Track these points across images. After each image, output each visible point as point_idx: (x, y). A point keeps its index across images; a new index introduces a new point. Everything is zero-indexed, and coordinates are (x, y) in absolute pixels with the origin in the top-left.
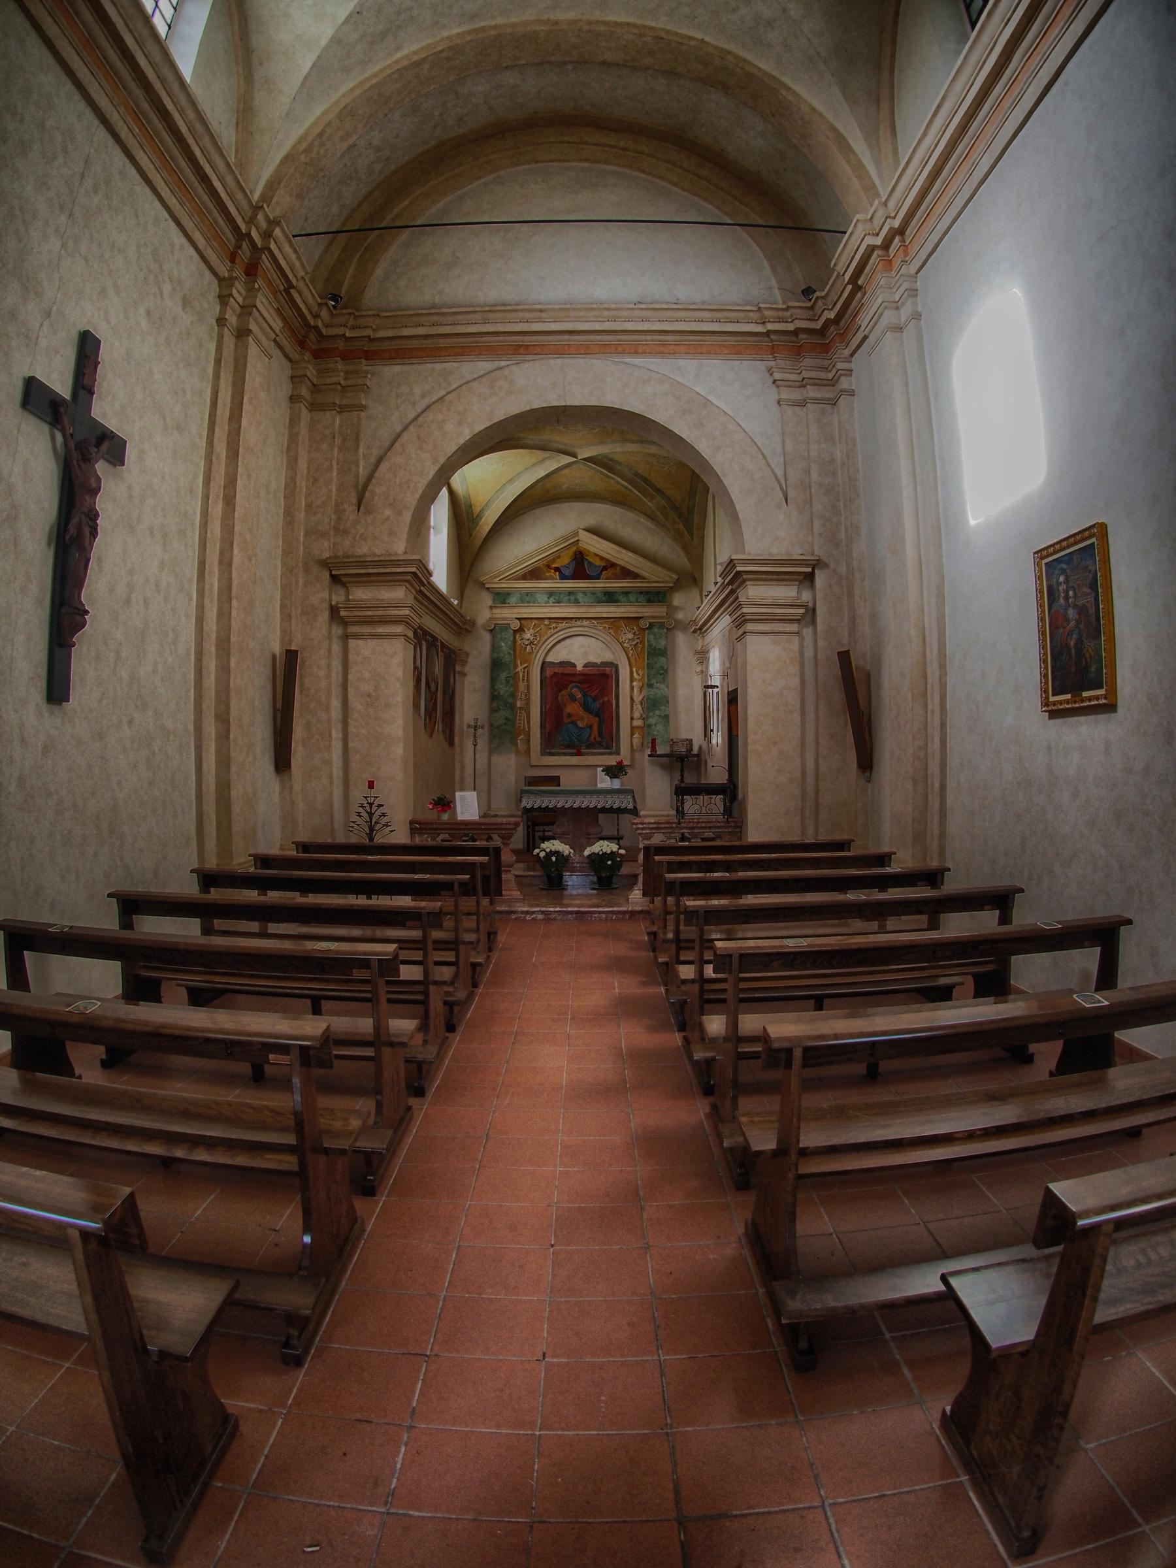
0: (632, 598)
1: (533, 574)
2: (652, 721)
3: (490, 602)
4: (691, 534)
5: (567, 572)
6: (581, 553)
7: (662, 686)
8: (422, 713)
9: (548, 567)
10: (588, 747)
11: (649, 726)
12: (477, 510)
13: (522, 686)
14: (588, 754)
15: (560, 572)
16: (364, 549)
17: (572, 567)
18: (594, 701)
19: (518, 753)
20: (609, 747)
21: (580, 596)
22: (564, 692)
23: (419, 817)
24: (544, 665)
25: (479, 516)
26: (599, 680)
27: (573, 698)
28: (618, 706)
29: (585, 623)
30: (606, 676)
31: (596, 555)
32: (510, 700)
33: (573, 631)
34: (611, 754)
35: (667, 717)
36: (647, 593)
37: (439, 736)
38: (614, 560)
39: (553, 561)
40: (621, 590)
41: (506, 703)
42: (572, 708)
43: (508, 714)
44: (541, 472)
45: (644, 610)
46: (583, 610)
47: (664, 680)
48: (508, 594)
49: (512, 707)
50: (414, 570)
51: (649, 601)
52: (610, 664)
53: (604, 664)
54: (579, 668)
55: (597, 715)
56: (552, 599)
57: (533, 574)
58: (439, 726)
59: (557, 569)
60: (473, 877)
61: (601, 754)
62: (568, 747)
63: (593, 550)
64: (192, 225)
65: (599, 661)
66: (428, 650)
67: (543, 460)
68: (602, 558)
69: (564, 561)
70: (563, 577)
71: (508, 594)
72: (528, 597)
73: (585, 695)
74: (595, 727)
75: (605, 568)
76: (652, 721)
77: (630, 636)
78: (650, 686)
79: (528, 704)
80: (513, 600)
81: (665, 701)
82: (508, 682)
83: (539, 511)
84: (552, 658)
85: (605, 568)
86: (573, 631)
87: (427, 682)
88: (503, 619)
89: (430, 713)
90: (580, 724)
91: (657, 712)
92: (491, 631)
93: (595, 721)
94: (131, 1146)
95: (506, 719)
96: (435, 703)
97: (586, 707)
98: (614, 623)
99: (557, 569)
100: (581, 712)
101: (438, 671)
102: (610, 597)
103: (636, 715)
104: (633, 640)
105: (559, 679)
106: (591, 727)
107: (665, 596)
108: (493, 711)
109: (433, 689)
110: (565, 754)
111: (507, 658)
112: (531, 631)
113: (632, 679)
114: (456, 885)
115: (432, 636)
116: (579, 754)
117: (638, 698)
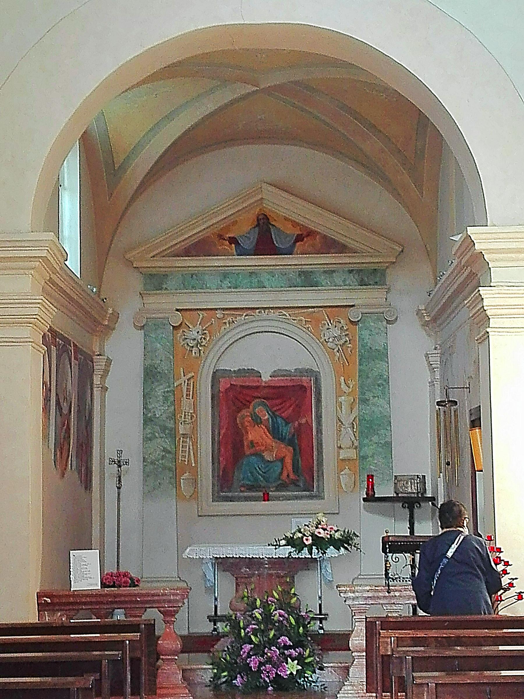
0: (338, 279)
1: (200, 248)
2: (368, 451)
3: (140, 287)
4: (419, 185)
5: (248, 244)
6: (266, 218)
7: (381, 402)
8: (52, 446)
9: (221, 237)
10: (279, 488)
11: (364, 458)
12: (119, 159)
13: (186, 405)
14: (278, 498)
15: (237, 243)
16: (416, 522)
17: (254, 236)
18: (287, 423)
19: (180, 497)
20: (309, 488)
21: (265, 278)
22: (244, 412)
23: (47, 588)
24: (216, 376)
25: (123, 168)
26: (293, 397)
27: (257, 421)
28: (319, 431)
29: (273, 314)
30: (303, 389)
31: (286, 219)
32: (170, 424)
33: (256, 326)
34: (311, 497)
35: (388, 445)
36: (359, 271)
37: (72, 474)
38: (312, 227)
39: (227, 229)
40: (321, 268)
41: (164, 428)
42: (256, 434)
43: (167, 444)
44: (209, 106)
45: (354, 295)
46: (272, 296)
47: (383, 393)
48: (166, 276)
49: (173, 434)
50: (44, 254)
51: (362, 283)
52: (309, 372)
53: (301, 372)
54: (266, 378)
55: (291, 443)
56: (226, 282)
57: (200, 248)
58: (73, 461)
59: (233, 240)
60: (124, 653)
61: (297, 498)
62: (250, 488)
63: (282, 212)
64: (419, 673)
65: (292, 368)
66: (59, 357)
67: (212, 91)
68: (295, 224)
69: (245, 229)
70: (242, 252)
71: (166, 276)
72: (192, 281)
73: (274, 416)
74: (288, 461)
75: (299, 238)
76: (368, 451)
77: (337, 332)
78: (364, 401)
79: (194, 430)
80: (171, 284)
81: (386, 422)
82: (166, 399)
83: (208, 157)
84: (231, 363)
85: (299, 238)
86: (256, 326)
87: (58, 403)
88: (159, 311)
89: (61, 446)
90: (268, 457)
91: (375, 439)
92: (142, 328)
93: (287, 452)
94: (240, 268)
95: (165, 450)
96: (68, 428)
97: (275, 432)
98: (312, 316)
99: (233, 240)
100: (269, 440)
101: (71, 386)
102: (307, 279)
103: (345, 443)
104: (340, 338)
105: (237, 395)
106: (282, 460)
107: (383, 273)
108: (147, 439)
109: (65, 411)
110: (247, 499)
111: (164, 367)
112: (199, 328)
113: (339, 393)
114: (105, 662)
115: (63, 338)
116: (266, 498)
117: (347, 419)
